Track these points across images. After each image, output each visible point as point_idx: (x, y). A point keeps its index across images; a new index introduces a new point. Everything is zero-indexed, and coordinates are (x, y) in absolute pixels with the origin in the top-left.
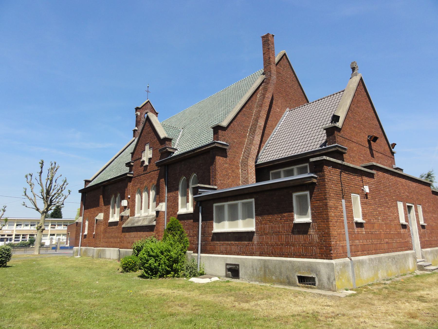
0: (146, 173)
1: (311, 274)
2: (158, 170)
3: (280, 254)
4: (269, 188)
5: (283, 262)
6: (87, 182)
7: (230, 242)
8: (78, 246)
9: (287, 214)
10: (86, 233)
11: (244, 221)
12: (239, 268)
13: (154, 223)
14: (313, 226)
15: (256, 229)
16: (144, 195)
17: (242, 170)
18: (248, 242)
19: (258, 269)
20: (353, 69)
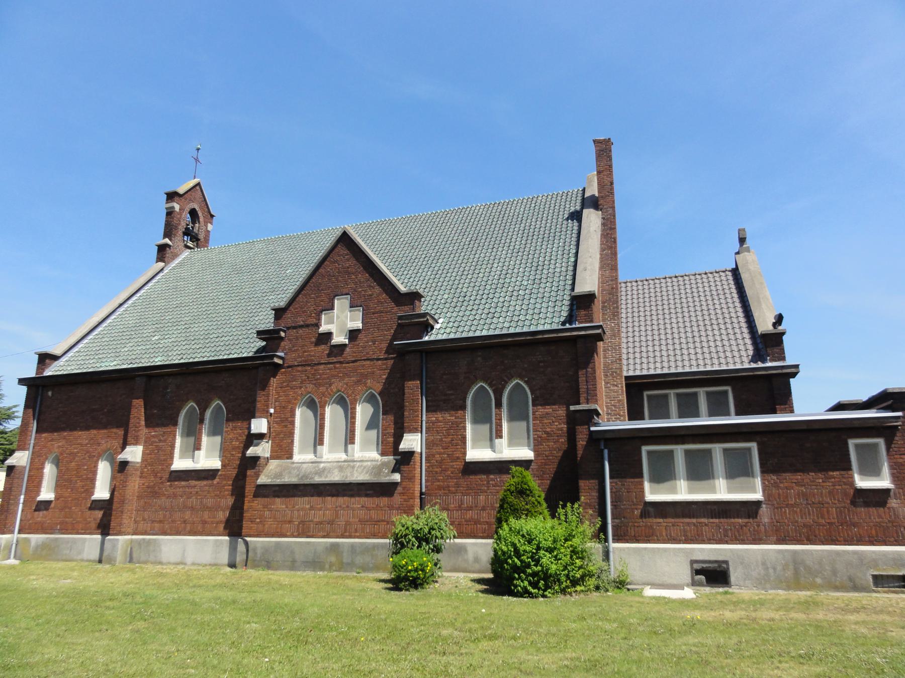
0: (341, 363)
1: (900, 570)
2: (386, 359)
3: (295, 534)
4: (805, 427)
5: (838, 553)
6: (45, 359)
7: (694, 520)
8: (12, 532)
9: (838, 473)
10: (46, 494)
11: (731, 481)
12: (728, 568)
13: (397, 477)
14: (895, 494)
15: (764, 495)
16: (332, 413)
17: (607, 383)
18: (746, 520)
19: (779, 568)
20: (742, 240)
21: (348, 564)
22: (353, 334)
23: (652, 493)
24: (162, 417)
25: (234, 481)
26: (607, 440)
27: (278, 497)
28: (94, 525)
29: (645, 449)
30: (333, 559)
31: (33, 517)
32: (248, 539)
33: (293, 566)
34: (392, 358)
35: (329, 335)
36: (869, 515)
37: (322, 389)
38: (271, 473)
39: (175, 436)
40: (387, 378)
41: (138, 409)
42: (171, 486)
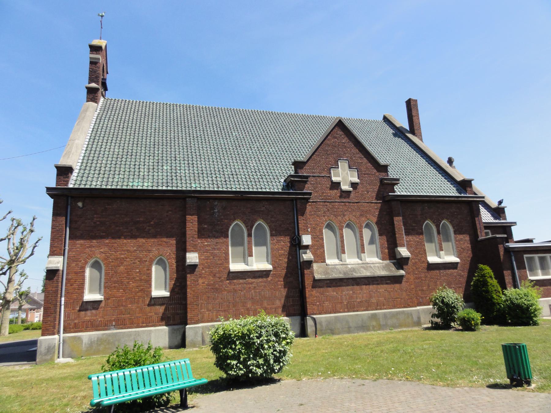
21: (384, 325)
22: (354, 185)
23: (531, 276)
24: (213, 229)
25: (284, 279)
26: (514, 252)
27: (330, 287)
28: (155, 318)
29: (525, 256)
30: (374, 323)
31: (79, 317)
32: (314, 316)
33: (349, 330)
34: (379, 203)
35: (339, 184)
36: (88, 315)
37: (340, 218)
38: (318, 271)
39: (228, 246)
40: (379, 215)
41: (192, 223)
42: (230, 284)
